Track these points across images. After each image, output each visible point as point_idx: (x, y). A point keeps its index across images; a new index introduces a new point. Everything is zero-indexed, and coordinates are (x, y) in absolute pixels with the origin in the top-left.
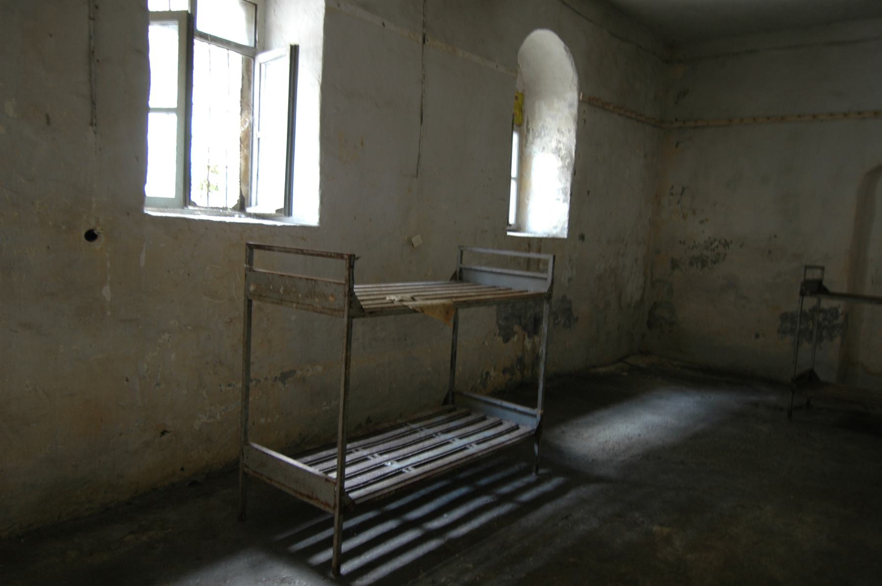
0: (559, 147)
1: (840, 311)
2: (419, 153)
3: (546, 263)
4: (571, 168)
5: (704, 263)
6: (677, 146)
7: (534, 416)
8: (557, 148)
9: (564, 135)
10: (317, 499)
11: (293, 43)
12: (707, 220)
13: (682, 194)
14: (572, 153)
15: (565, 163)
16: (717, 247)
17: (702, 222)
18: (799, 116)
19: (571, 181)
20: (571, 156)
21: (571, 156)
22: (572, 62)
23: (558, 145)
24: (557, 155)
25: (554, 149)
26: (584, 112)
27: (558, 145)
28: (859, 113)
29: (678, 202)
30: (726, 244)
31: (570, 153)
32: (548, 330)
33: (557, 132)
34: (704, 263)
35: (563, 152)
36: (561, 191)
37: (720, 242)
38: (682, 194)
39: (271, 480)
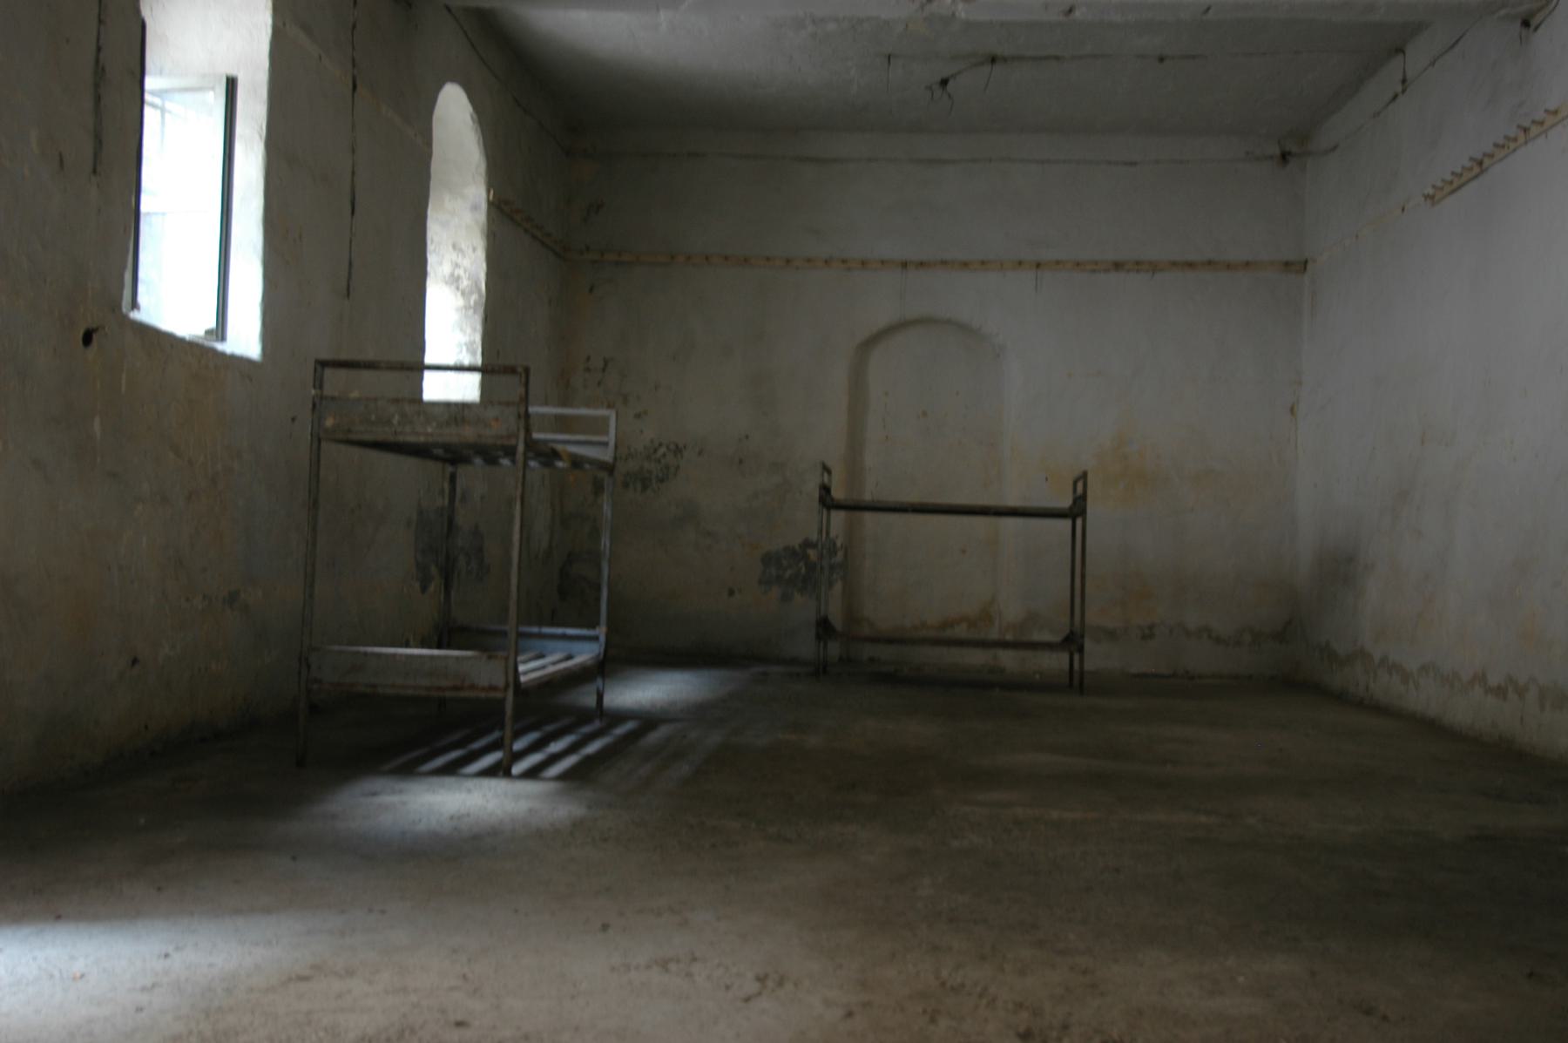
0: (456, 274)
1: (839, 544)
3: (606, 420)
4: (481, 310)
5: (645, 483)
7: (596, 639)
8: (452, 275)
10: (473, 687)
11: (232, 72)
13: (604, 370)
14: (481, 283)
15: (469, 302)
16: (664, 455)
17: (638, 416)
18: (768, 259)
20: (479, 290)
21: (479, 290)
22: (479, 139)
23: (454, 270)
24: (453, 287)
25: (447, 276)
27: (454, 270)
28: (844, 261)
29: (599, 384)
30: (678, 451)
31: (476, 284)
33: (451, 248)
34: (645, 483)
35: (465, 283)
36: (464, 348)
37: (668, 448)
38: (604, 370)
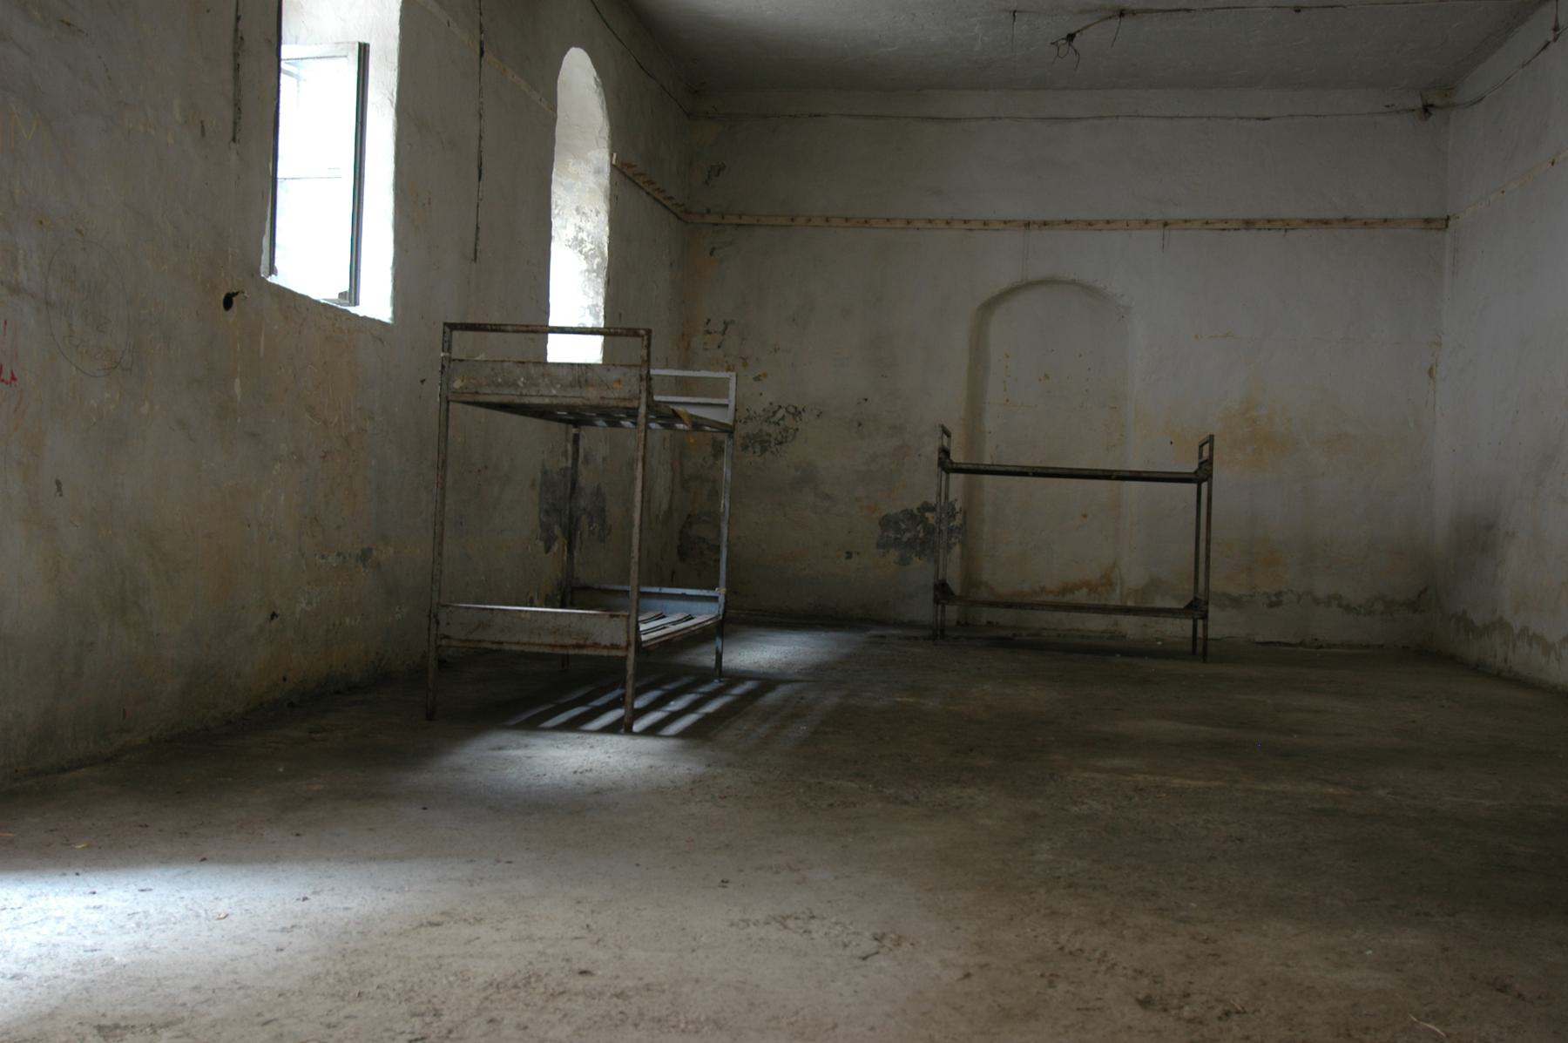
1: (958, 506)
2: (477, 225)
6: (711, 254)
7: (715, 599)
8: (576, 238)
9: (587, 217)
10: (596, 645)
11: (363, 40)
12: (765, 375)
13: (724, 333)
16: (784, 417)
17: (757, 379)
19: (604, 294)
21: (602, 253)
22: (603, 103)
26: (616, 184)
29: (719, 347)
30: (797, 413)
32: (732, 476)
33: (575, 213)
36: (588, 311)
39: (500, 643)
